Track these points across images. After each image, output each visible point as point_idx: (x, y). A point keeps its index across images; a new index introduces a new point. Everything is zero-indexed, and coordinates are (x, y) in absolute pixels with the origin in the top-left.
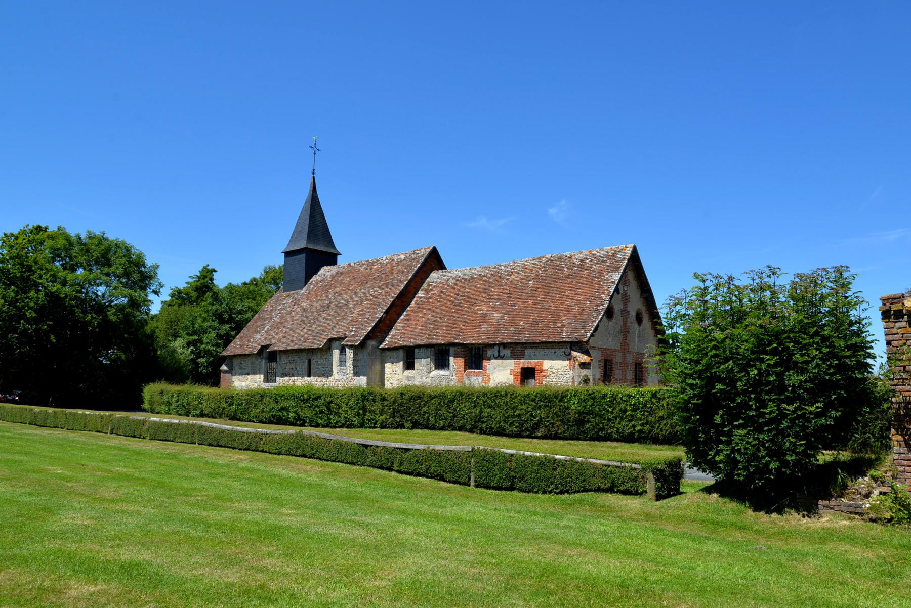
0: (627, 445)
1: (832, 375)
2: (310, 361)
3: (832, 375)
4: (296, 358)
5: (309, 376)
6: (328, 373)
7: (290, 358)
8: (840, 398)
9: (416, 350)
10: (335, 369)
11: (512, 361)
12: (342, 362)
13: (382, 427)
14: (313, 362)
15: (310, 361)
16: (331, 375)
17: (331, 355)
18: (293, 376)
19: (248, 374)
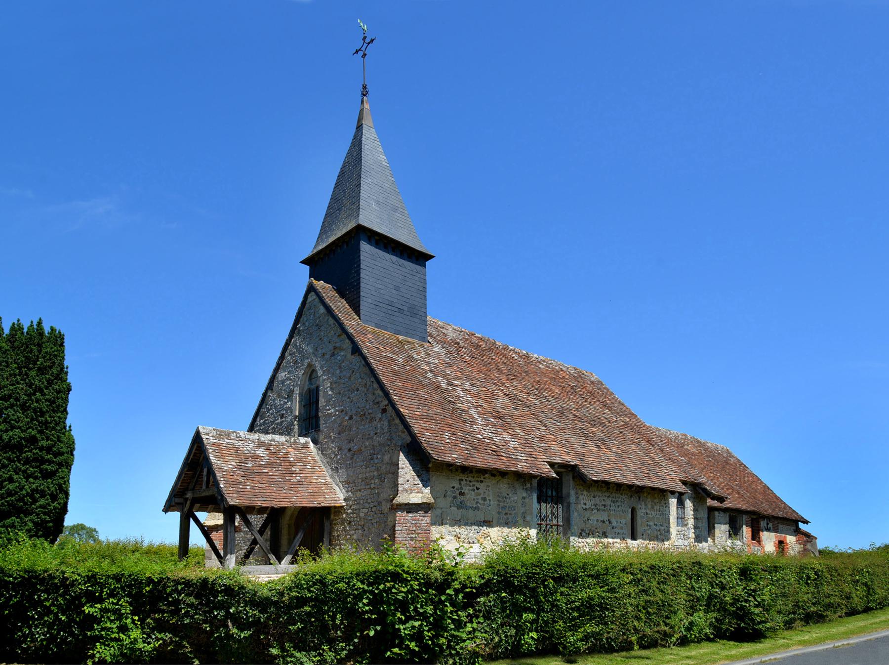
0: (816, 632)
1: (394, 587)
2: (633, 511)
3: (394, 587)
4: (608, 502)
5: (634, 538)
6: (664, 535)
7: (597, 500)
8: (64, 640)
9: (717, 513)
10: (674, 529)
11: (773, 534)
12: (681, 519)
13: (684, 642)
14: (640, 513)
15: (633, 511)
16: (668, 539)
17: (667, 505)
18: (605, 535)
19: (488, 523)
